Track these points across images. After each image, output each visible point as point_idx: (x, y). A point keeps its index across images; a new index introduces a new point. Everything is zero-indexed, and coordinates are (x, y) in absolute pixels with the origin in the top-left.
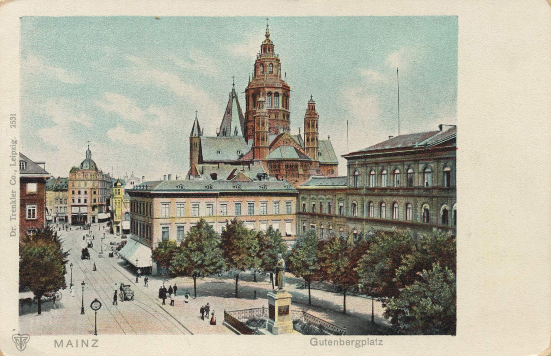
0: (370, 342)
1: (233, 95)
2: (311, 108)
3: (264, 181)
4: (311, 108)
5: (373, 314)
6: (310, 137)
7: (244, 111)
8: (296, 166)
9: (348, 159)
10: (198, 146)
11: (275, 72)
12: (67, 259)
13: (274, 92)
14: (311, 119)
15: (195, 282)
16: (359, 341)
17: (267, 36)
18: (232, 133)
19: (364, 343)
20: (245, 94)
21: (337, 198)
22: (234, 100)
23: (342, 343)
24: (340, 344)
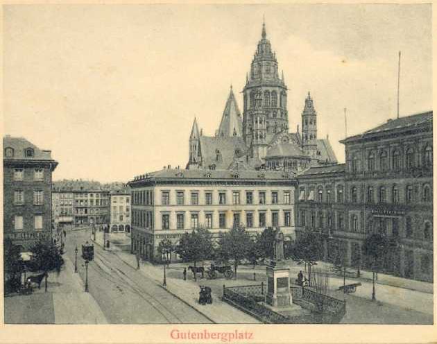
0: (238, 335)
1: (232, 97)
2: (309, 102)
3: (263, 171)
4: (309, 102)
5: (374, 294)
6: (309, 119)
7: (242, 111)
8: (295, 164)
9: (345, 144)
10: (197, 148)
11: (272, 71)
12: (60, 280)
13: (271, 91)
14: (309, 117)
15: (158, 206)
16: (226, 335)
17: (264, 34)
18: (231, 134)
19: (232, 336)
20: (242, 94)
21: (336, 185)
22: (233, 103)
23: (207, 336)
24: (205, 338)
